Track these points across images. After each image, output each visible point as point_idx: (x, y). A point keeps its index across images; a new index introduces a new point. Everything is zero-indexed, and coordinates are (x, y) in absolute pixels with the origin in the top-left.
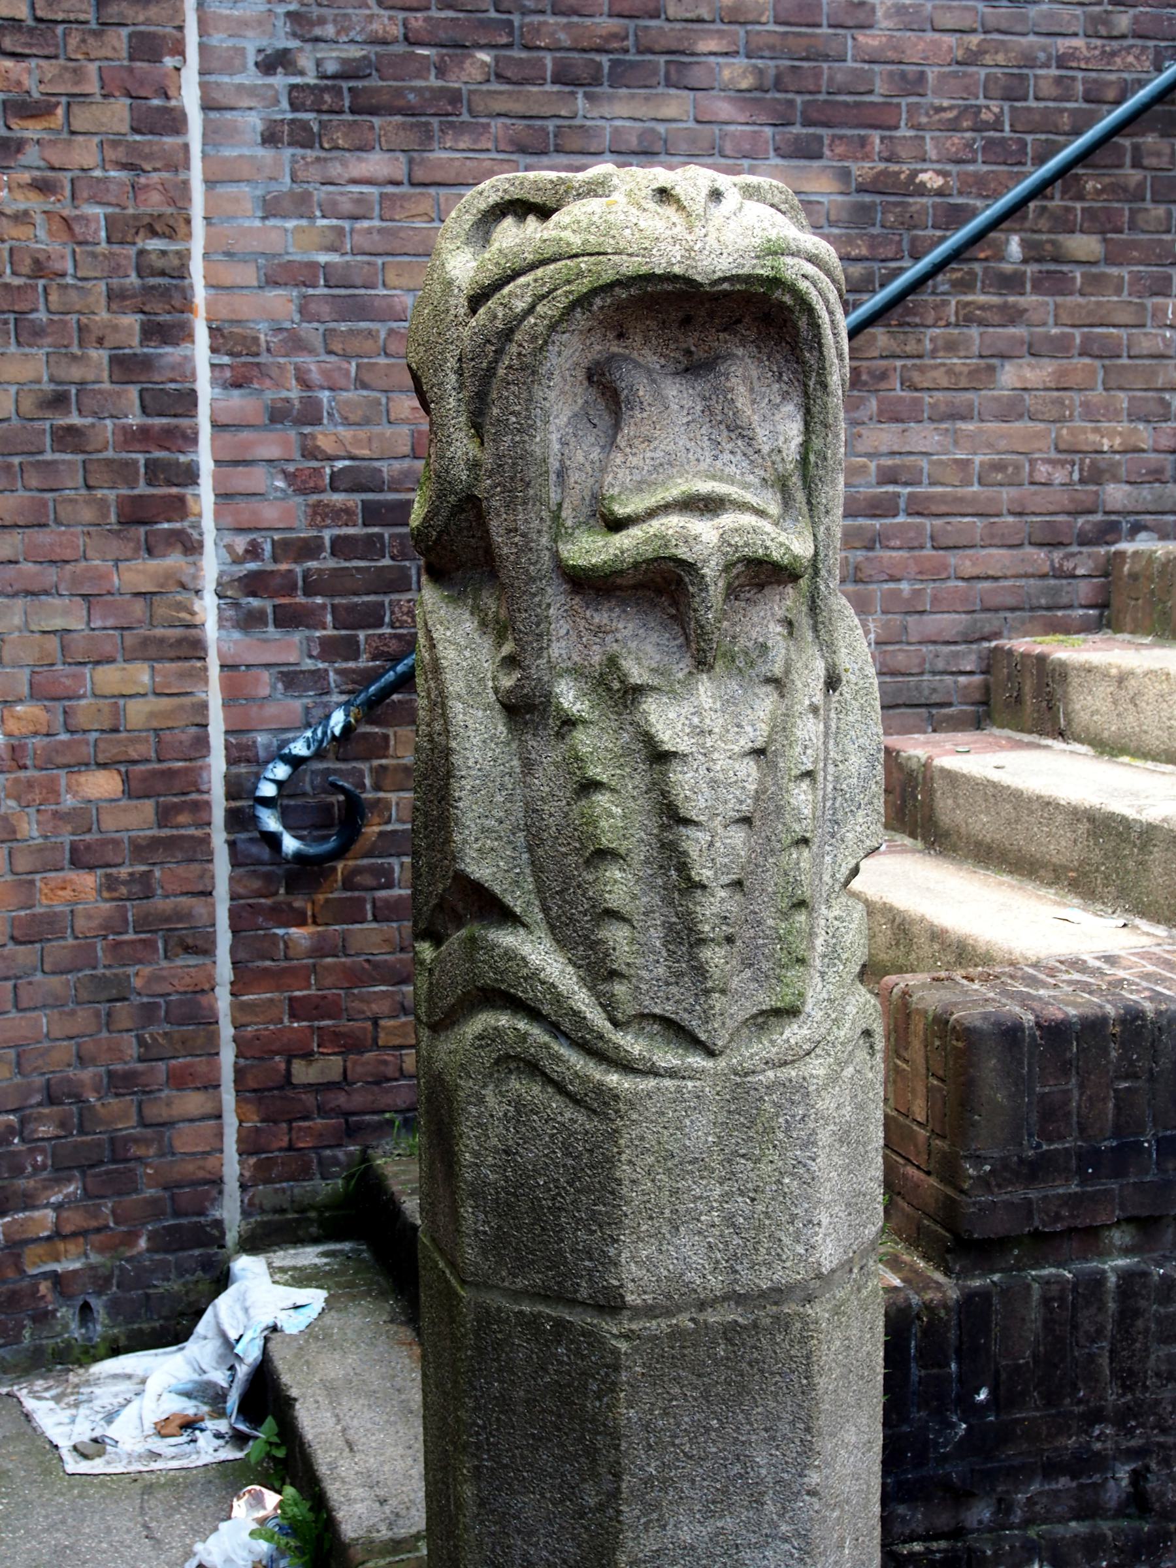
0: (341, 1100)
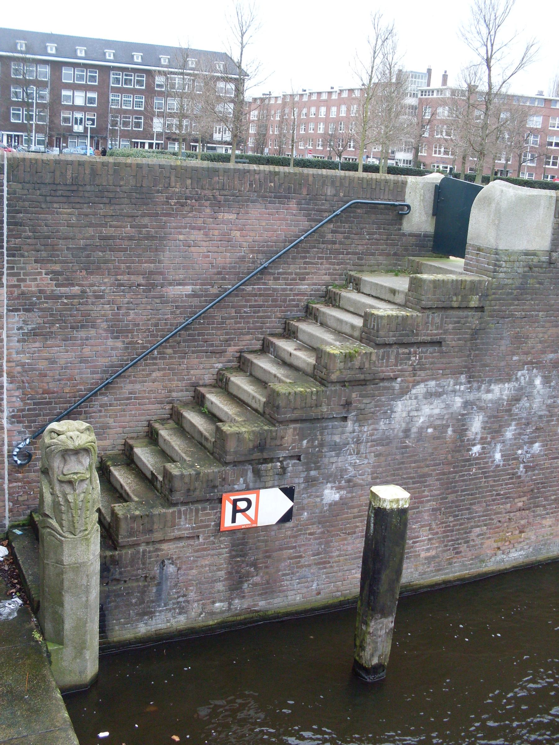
0: (27, 503)
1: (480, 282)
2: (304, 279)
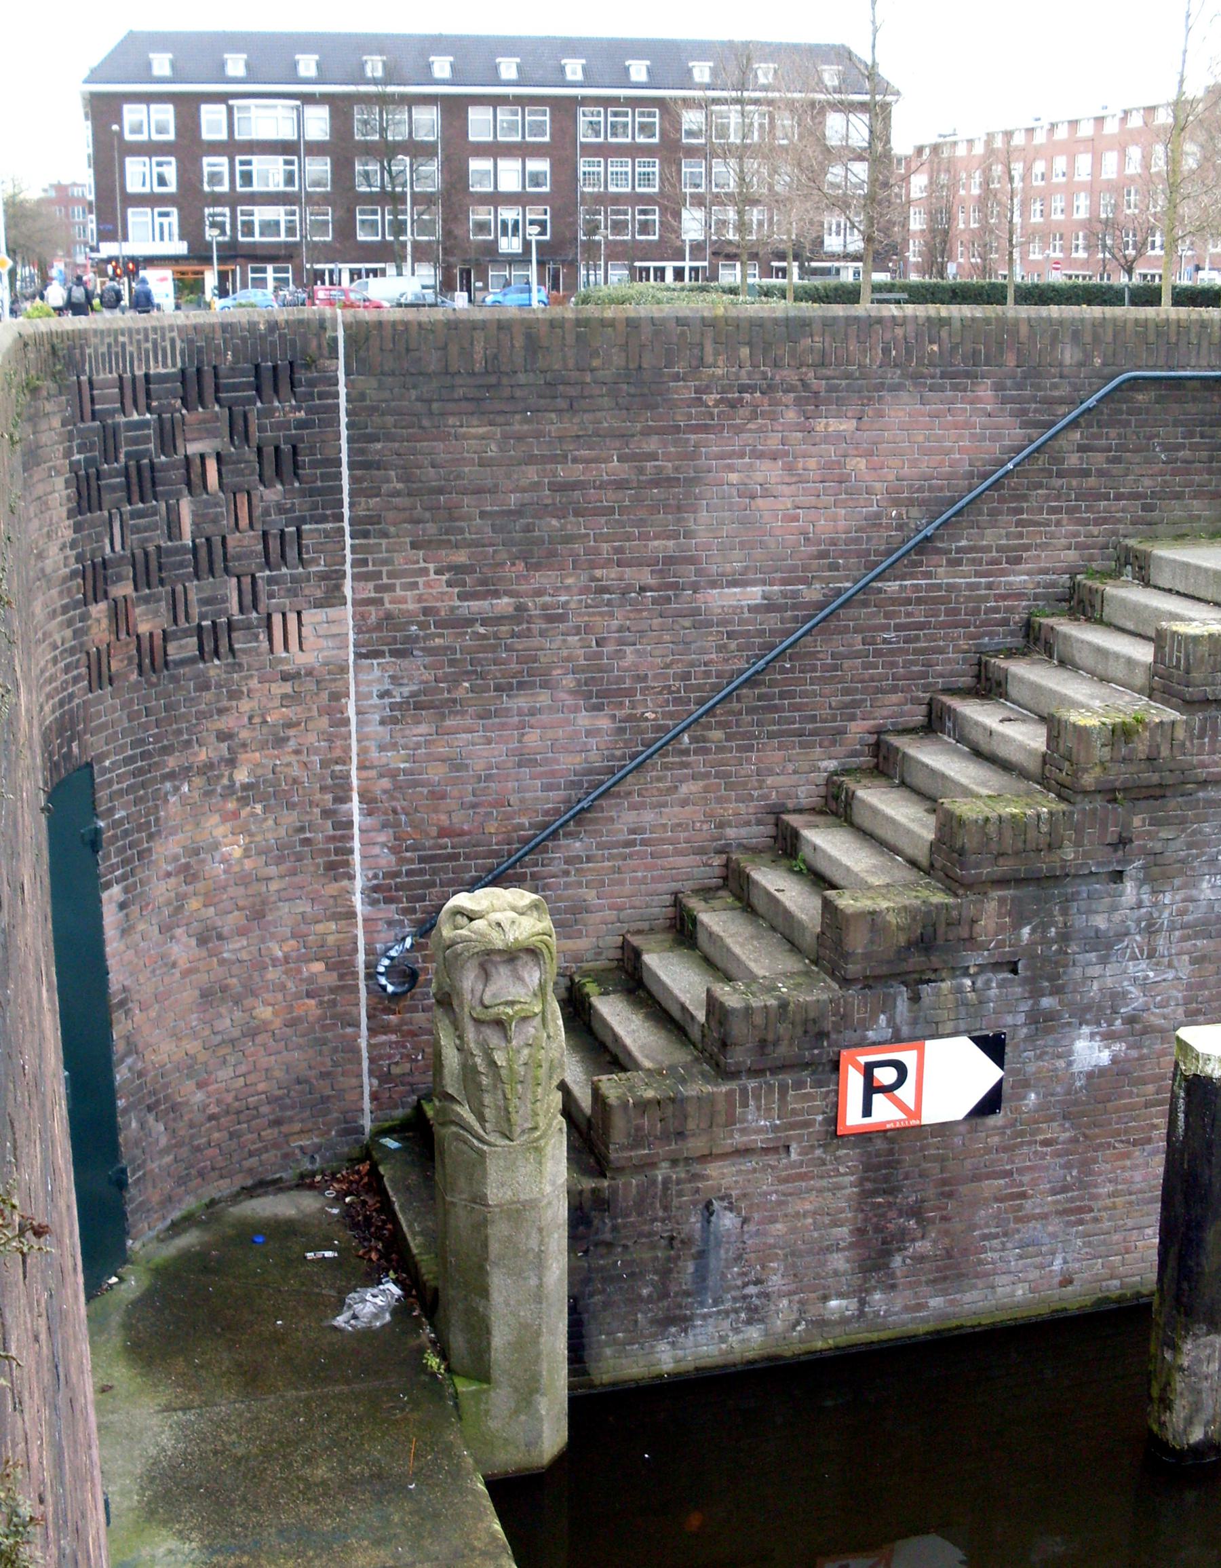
0: (410, 1079)
2: (1018, 560)
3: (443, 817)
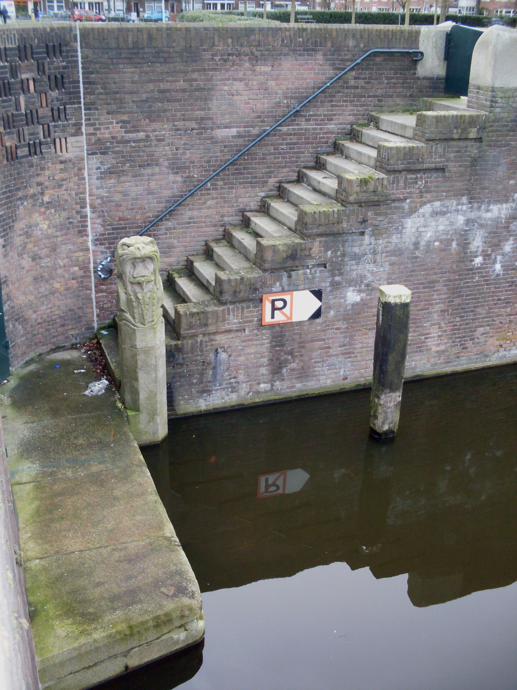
0: (111, 309)
1: (478, 116)
2: (331, 120)
3: (121, 213)
